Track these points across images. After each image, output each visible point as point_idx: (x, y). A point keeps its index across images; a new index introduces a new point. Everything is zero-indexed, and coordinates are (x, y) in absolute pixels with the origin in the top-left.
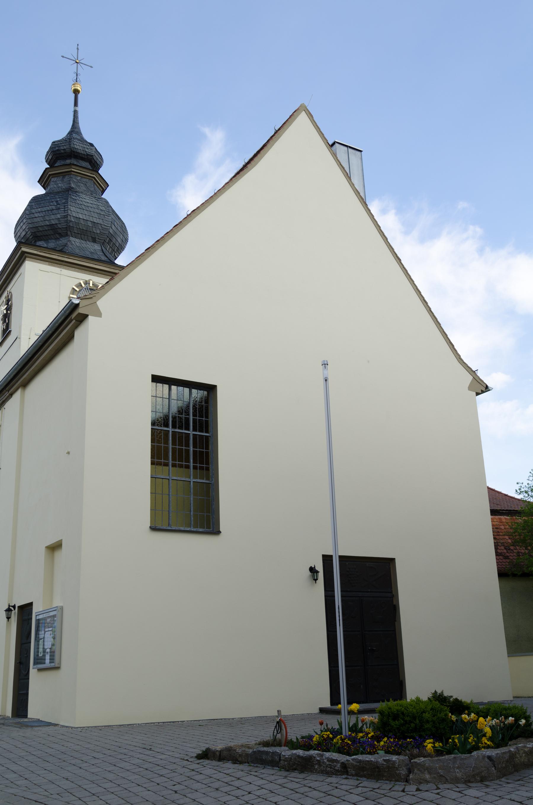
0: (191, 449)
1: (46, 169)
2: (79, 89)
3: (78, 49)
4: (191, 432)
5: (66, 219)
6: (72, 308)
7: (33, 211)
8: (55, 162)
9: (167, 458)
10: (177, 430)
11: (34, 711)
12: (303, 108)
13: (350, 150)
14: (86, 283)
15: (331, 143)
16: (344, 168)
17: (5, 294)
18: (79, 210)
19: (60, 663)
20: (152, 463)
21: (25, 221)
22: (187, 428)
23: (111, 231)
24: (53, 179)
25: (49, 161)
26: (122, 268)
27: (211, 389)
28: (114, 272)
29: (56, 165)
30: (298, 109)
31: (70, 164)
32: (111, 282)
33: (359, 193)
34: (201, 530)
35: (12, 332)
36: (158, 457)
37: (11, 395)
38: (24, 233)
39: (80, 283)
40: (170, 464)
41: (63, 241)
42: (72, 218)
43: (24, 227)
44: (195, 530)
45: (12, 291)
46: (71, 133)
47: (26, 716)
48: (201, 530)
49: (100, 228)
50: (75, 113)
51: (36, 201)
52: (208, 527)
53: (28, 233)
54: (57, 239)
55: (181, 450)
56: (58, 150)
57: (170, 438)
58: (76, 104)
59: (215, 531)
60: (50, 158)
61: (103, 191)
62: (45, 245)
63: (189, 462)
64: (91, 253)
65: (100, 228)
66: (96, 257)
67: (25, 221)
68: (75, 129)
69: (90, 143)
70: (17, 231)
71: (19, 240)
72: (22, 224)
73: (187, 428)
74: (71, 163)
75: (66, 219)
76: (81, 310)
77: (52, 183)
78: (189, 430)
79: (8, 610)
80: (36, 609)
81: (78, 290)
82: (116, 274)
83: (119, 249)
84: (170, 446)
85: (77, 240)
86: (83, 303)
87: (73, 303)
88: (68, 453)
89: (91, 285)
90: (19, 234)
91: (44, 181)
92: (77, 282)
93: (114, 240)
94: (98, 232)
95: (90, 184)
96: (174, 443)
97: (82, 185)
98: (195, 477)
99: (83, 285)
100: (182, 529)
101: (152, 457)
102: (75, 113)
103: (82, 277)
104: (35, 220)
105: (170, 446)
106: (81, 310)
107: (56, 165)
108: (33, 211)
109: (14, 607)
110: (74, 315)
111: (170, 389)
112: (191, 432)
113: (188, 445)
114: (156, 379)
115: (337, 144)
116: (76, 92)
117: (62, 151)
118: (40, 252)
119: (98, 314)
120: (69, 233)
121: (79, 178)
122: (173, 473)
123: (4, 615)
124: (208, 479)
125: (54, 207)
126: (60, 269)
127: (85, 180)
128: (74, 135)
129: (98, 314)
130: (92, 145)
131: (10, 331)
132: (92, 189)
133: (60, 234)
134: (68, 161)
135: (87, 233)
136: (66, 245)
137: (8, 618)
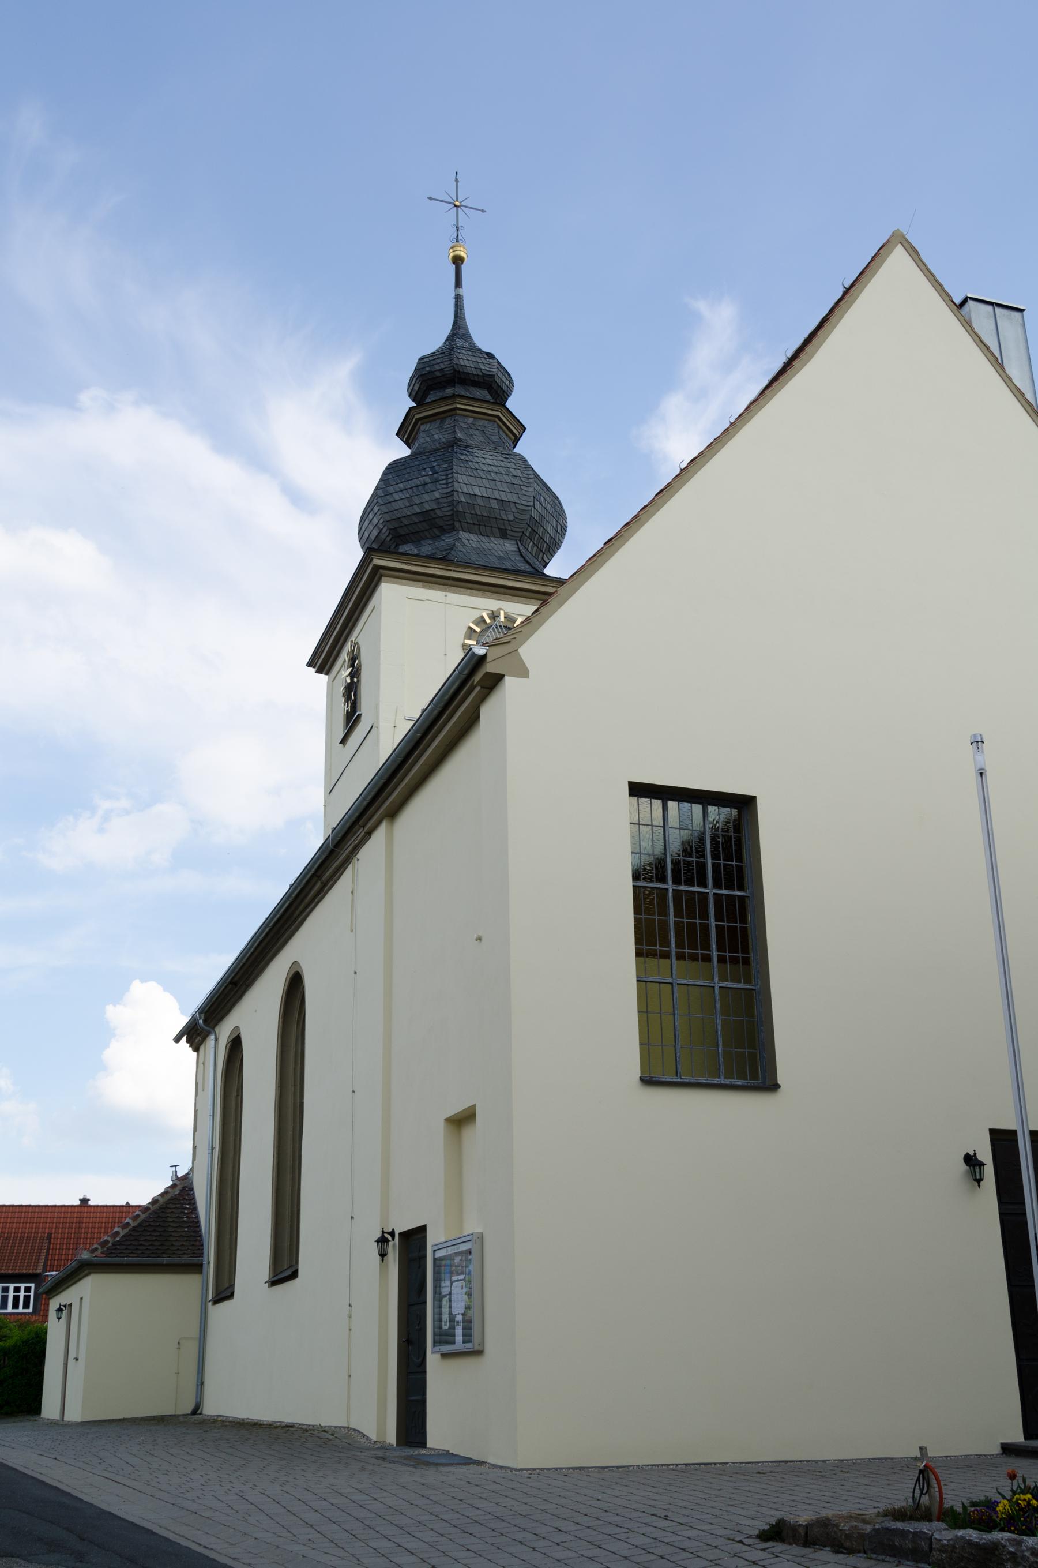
0: (713, 922)
1: (411, 409)
2: (462, 254)
3: (457, 181)
4: (710, 890)
5: (450, 499)
6: (473, 664)
7: (391, 489)
8: (425, 395)
9: (665, 942)
10: (683, 887)
11: (439, 1434)
12: (898, 239)
13: (998, 310)
14: (494, 616)
15: (958, 301)
16: (988, 348)
17: (347, 647)
18: (473, 481)
19: (482, 1343)
20: (639, 954)
21: (376, 509)
22: (703, 883)
23: (534, 514)
24: (423, 428)
25: (414, 393)
26: (561, 582)
27: (745, 804)
28: (546, 593)
29: (428, 400)
30: (888, 241)
31: (454, 396)
32: (543, 610)
33: (1023, 394)
34: (739, 1082)
35: (362, 718)
36: (648, 941)
37: (369, 834)
38: (375, 533)
39: (482, 617)
40: (673, 954)
41: (447, 540)
42: (461, 495)
43: (375, 521)
44: (728, 1082)
45: (360, 641)
46: (451, 338)
47: (423, 1444)
48: (739, 1082)
49: (514, 510)
50: (458, 298)
51: (394, 470)
52: (754, 1077)
53: (384, 531)
54: (435, 537)
55: (692, 927)
56: (430, 372)
57: (671, 904)
58: (458, 284)
59: (768, 1083)
60: (416, 388)
61: (516, 440)
62: (415, 551)
63: (709, 948)
64: (500, 558)
65: (514, 510)
66: (508, 565)
67: (376, 509)
68: (459, 329)
69: (487, 353)
70: (366, 523)
71: (367, 545)
72: (371, 516)
73: (703, 883)
74: (456, 395)
75: (450, 499)
76: (490, 667)
77: (422, 434)
78: (705, 886)
79: (382, 1241)
80: (432, 1239)
81: (478, 629)
82: (550, 594)
83: (551, 547)
84: (672, 919)
85: (472, 537)
86: (494, 653)
87: (474, 654)
88: (479, 939)
89: (502, 619)
90: (366, 535)
91: (407, 432)
92: (476, 615)
93: (540, 531)
94: (511, 518)
95: (491, 429)
96: (678, 913)
97: (476, 432)
98: (723, 978)
99: (488, 621)
100: (703, 1080)
101: (638, 941)
102: (458, 298)
103: (484, 605)
104: (396, 506)
105: (672, 919)
106: (490, 667)
107: (428, 400)
108: (391, 489)
109: (392, 1234)
110: (477, 678)
111: (665, 808)
112: (710, 890)
113: (705, 916)
114: (638, 790)
115: (970, 302)
116: (458, 261)
117: (438, 374)
118: (407, 564)
119: (523, 672)
120: (457, 525)
121: (470, 420)
122: (679, 972)
123: (374, 1249)
124: (748, 981)
125: (427, 479)
126: (444, 593)
127: (481, 423)
128: (458, 342)
129: (523, 672)
130: (491, 356)
131: (359, 716)
132: (495, 439)
133: (440, 528)
134: (449, 391)
135: (490, 522)
136: (452, 547)
137: (383, 1255)
